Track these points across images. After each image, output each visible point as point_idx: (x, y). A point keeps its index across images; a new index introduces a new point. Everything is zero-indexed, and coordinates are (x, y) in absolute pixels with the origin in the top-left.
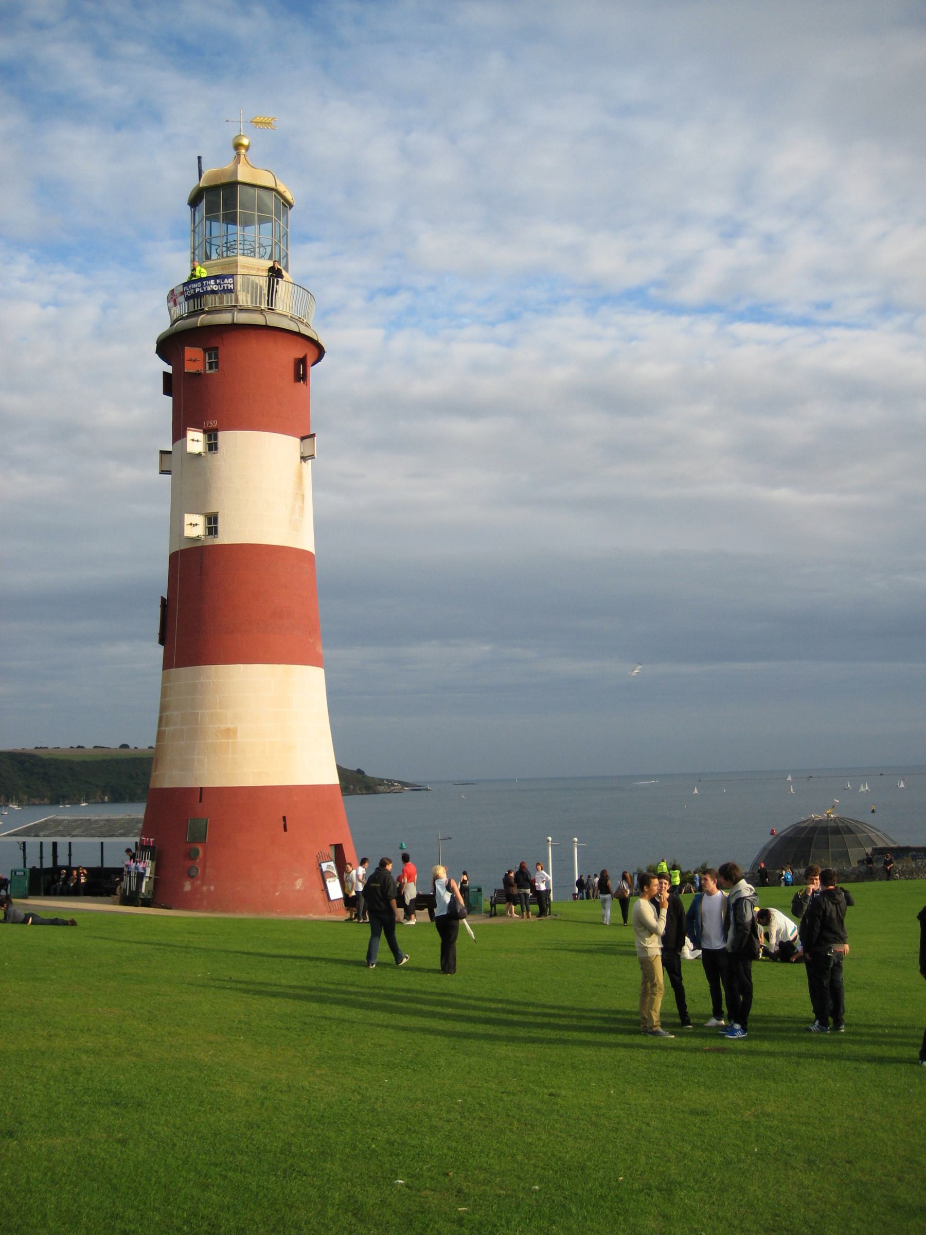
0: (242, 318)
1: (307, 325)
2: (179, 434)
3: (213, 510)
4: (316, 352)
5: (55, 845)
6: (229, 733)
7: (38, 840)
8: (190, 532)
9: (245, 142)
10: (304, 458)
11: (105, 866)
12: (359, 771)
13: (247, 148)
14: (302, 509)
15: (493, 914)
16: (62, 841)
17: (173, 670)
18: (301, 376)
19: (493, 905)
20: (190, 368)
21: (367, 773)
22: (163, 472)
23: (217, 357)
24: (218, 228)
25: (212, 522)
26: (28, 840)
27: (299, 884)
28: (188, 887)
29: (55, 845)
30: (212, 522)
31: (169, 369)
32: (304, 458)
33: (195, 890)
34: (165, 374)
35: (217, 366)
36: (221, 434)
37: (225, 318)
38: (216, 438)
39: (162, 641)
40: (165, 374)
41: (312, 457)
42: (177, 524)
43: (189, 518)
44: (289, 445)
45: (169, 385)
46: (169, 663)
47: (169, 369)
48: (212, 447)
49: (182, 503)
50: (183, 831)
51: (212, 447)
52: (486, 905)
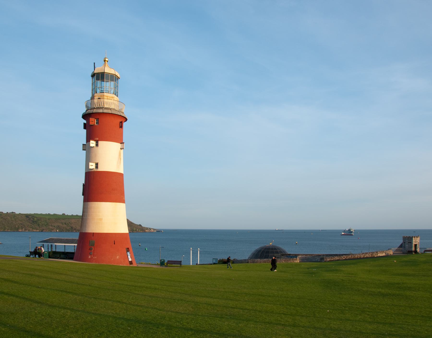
0: (105, 111)
1: (123, 113)
2: (88, 140)
3: (97, 162)
4: (125, 120)
5: (52, 246)
6: (101, 219)
7: (47, 244)
8: (91, 167)
9: (107, 60)
10: (121, 149)
11: (66, 251)
12: (140, 225)
13: (107, 61)
14: (120, 162)
15: (166, 266)
16: (50, 244)
17: (86, 203)
18: (121, 127)
19: (167, 264)
20: (91, 123)
21: (142, 226)
22: (83, 150)
23: (98, 121)
24: (99, 82)
25: (97, 165)
26: (44, 244)
27: (118, 257)
28: (90, 257)
29: (52, 246)
30: (97, 165)
31: (85, 122)
32: (121, 149)
33: (91, 258)
34: (84, 123)
35: (99, 124)
36: (99, 142)
37: (101, 111)
38: (98, 143)
39: (83, 195)
40: (84, 123)
41: (123, 148)
42: (87, 165)
43: (90, 164)
44: (118, 145)
45: (85, 126)
47: (85, 122)
48: (97, 145)
49: (88, 159)
50: (88, 243)
51: (97, 145)
52: (165, 264)
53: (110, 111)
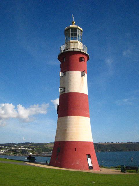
27: (78, 163)
46: (59, 117)
50: (61, 151)
53: (80, 51)
